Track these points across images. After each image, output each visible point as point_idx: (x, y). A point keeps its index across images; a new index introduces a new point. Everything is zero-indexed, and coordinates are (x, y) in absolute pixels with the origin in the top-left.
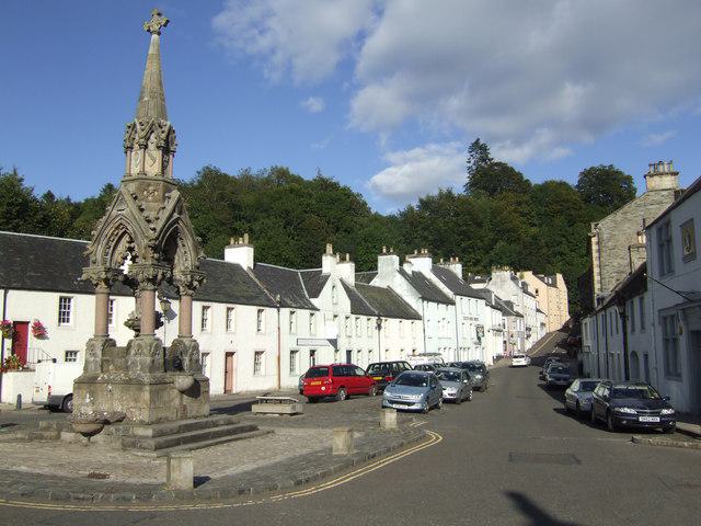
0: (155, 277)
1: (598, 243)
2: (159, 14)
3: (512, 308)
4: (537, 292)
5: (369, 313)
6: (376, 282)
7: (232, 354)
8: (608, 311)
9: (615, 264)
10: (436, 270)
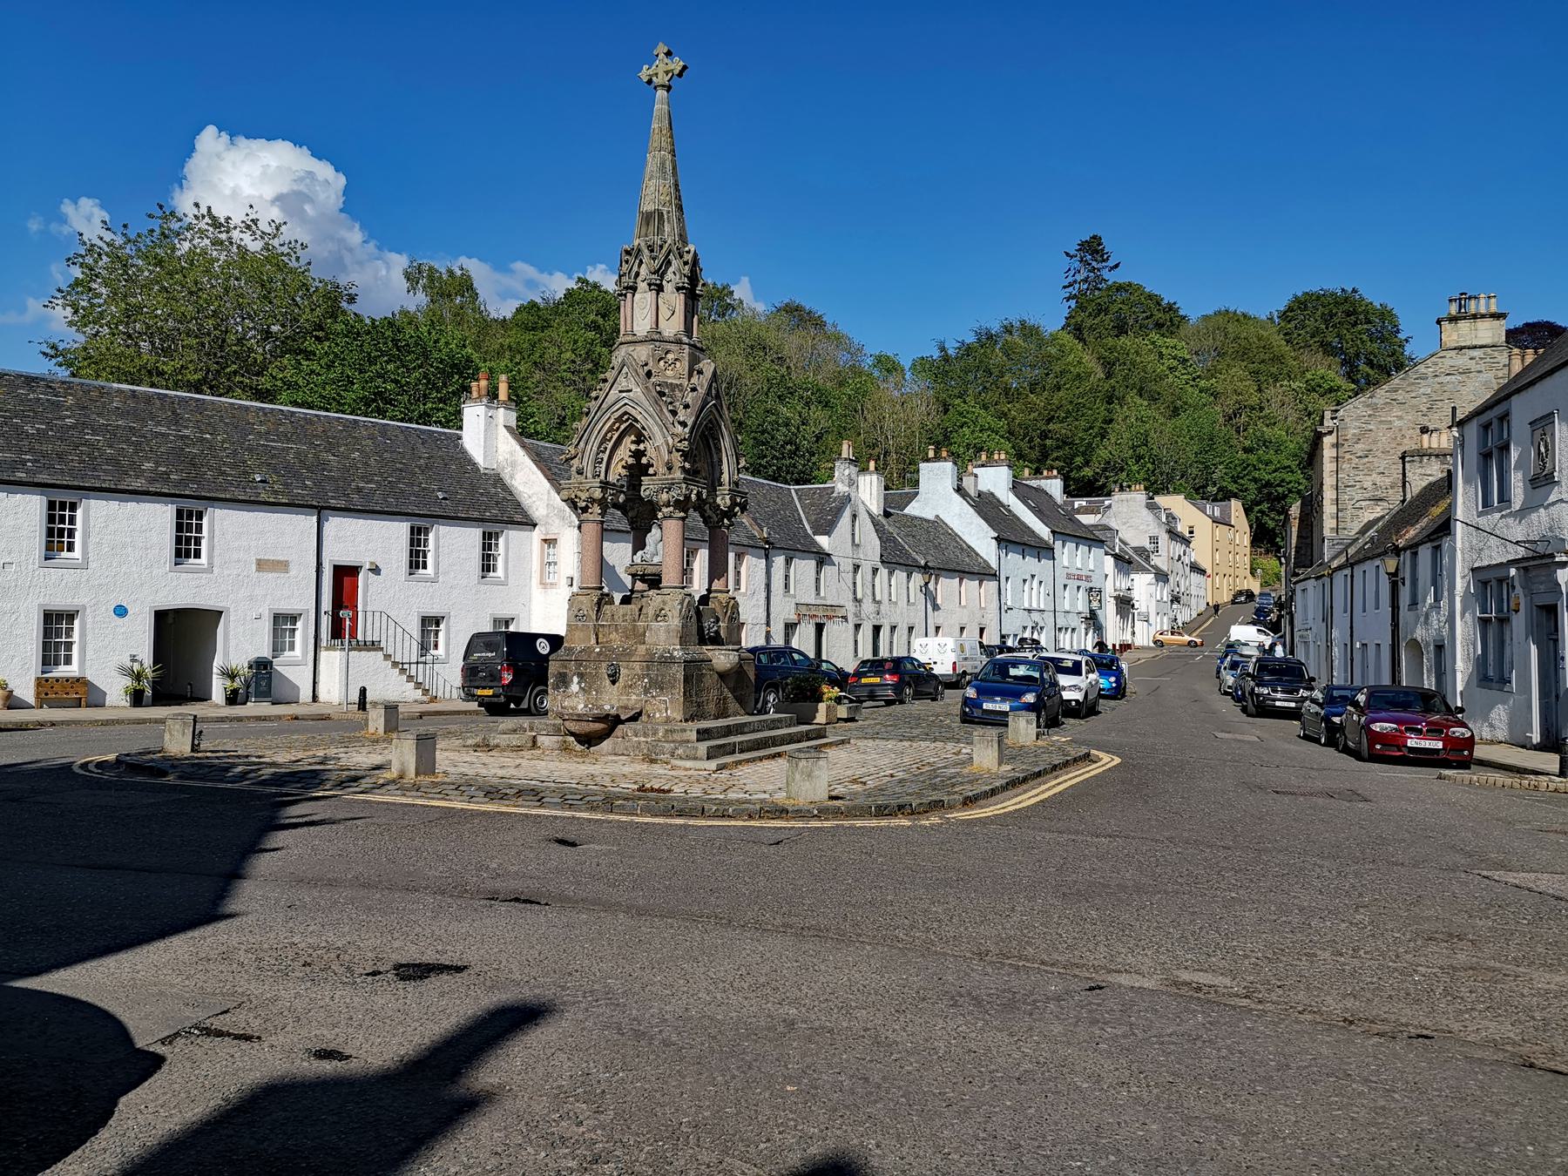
0: (688, 497)
1: (1337, 445)
2: (668, 54)
3: (1147, 559)
4: (1191, 532)
5: (910, 567)
6: (913, 509)
7: (437, 621)
8: (1358, 570)
9: (1368, 484)
10: (1017, 487)
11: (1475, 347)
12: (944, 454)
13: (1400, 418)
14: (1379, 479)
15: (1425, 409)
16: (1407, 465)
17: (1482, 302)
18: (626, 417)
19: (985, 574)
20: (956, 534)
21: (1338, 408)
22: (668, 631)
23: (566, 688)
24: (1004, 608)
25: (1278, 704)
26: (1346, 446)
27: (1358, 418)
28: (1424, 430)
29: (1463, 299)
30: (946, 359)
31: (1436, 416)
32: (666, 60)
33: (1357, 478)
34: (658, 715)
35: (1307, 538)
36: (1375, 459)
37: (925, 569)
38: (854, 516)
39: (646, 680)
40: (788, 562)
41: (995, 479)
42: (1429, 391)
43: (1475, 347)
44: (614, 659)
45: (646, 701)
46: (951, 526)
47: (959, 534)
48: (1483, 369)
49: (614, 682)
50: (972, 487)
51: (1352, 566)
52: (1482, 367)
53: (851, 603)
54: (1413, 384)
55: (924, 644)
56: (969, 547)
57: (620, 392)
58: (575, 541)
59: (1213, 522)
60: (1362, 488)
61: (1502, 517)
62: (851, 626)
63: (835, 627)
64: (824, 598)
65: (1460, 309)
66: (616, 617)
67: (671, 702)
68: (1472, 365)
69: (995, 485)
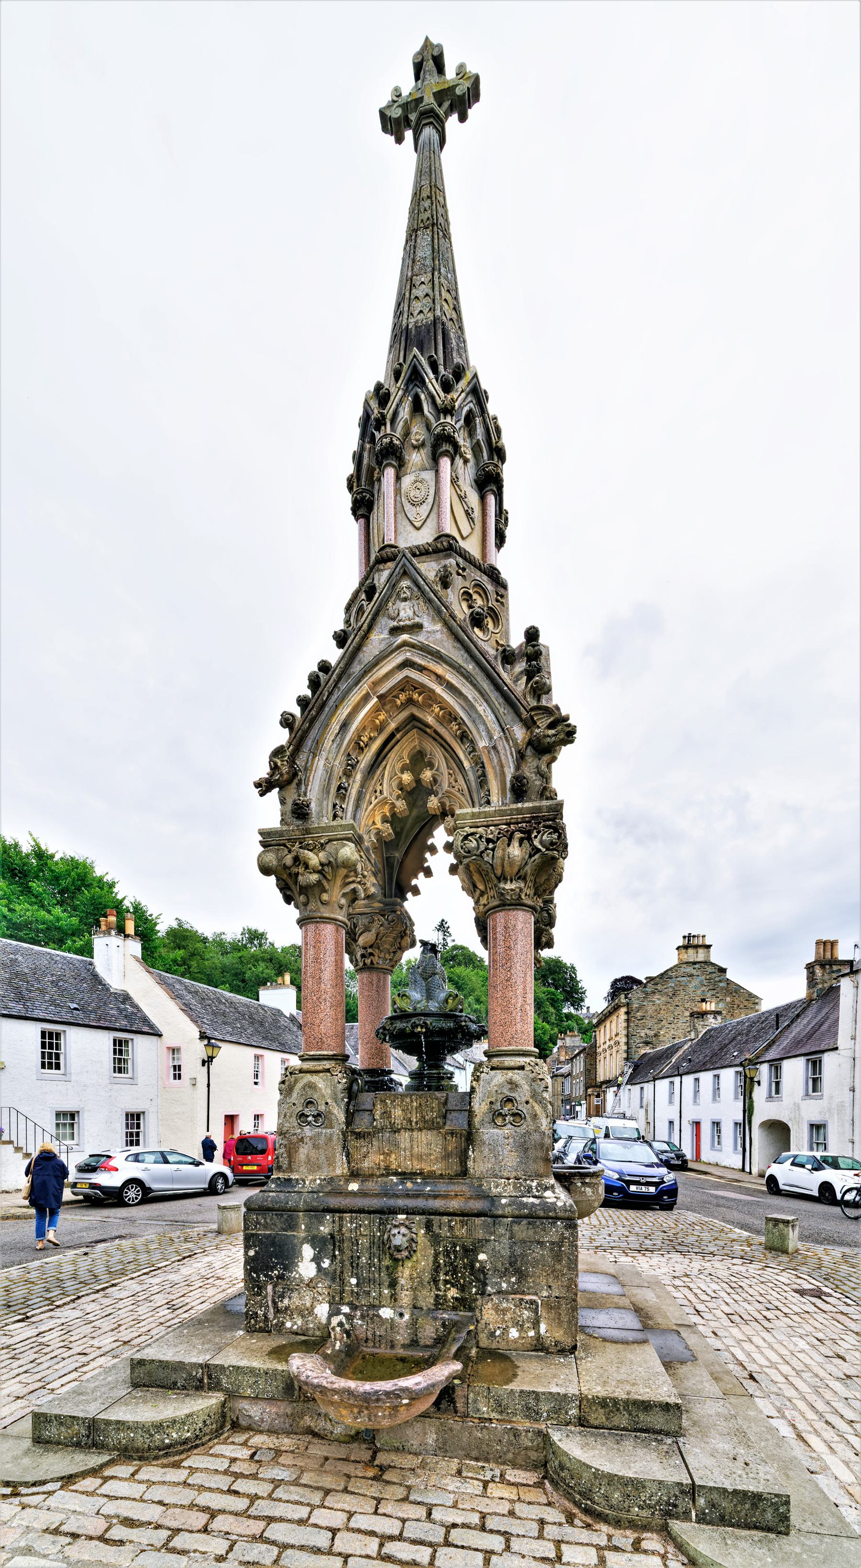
9: (643, 1035)
13: (659, 999)
14: (648, 1032)
23: (286, 1268)
27: (638, 999)
34: (514, 1333)
52: (699, 973)
68: (694, 972)
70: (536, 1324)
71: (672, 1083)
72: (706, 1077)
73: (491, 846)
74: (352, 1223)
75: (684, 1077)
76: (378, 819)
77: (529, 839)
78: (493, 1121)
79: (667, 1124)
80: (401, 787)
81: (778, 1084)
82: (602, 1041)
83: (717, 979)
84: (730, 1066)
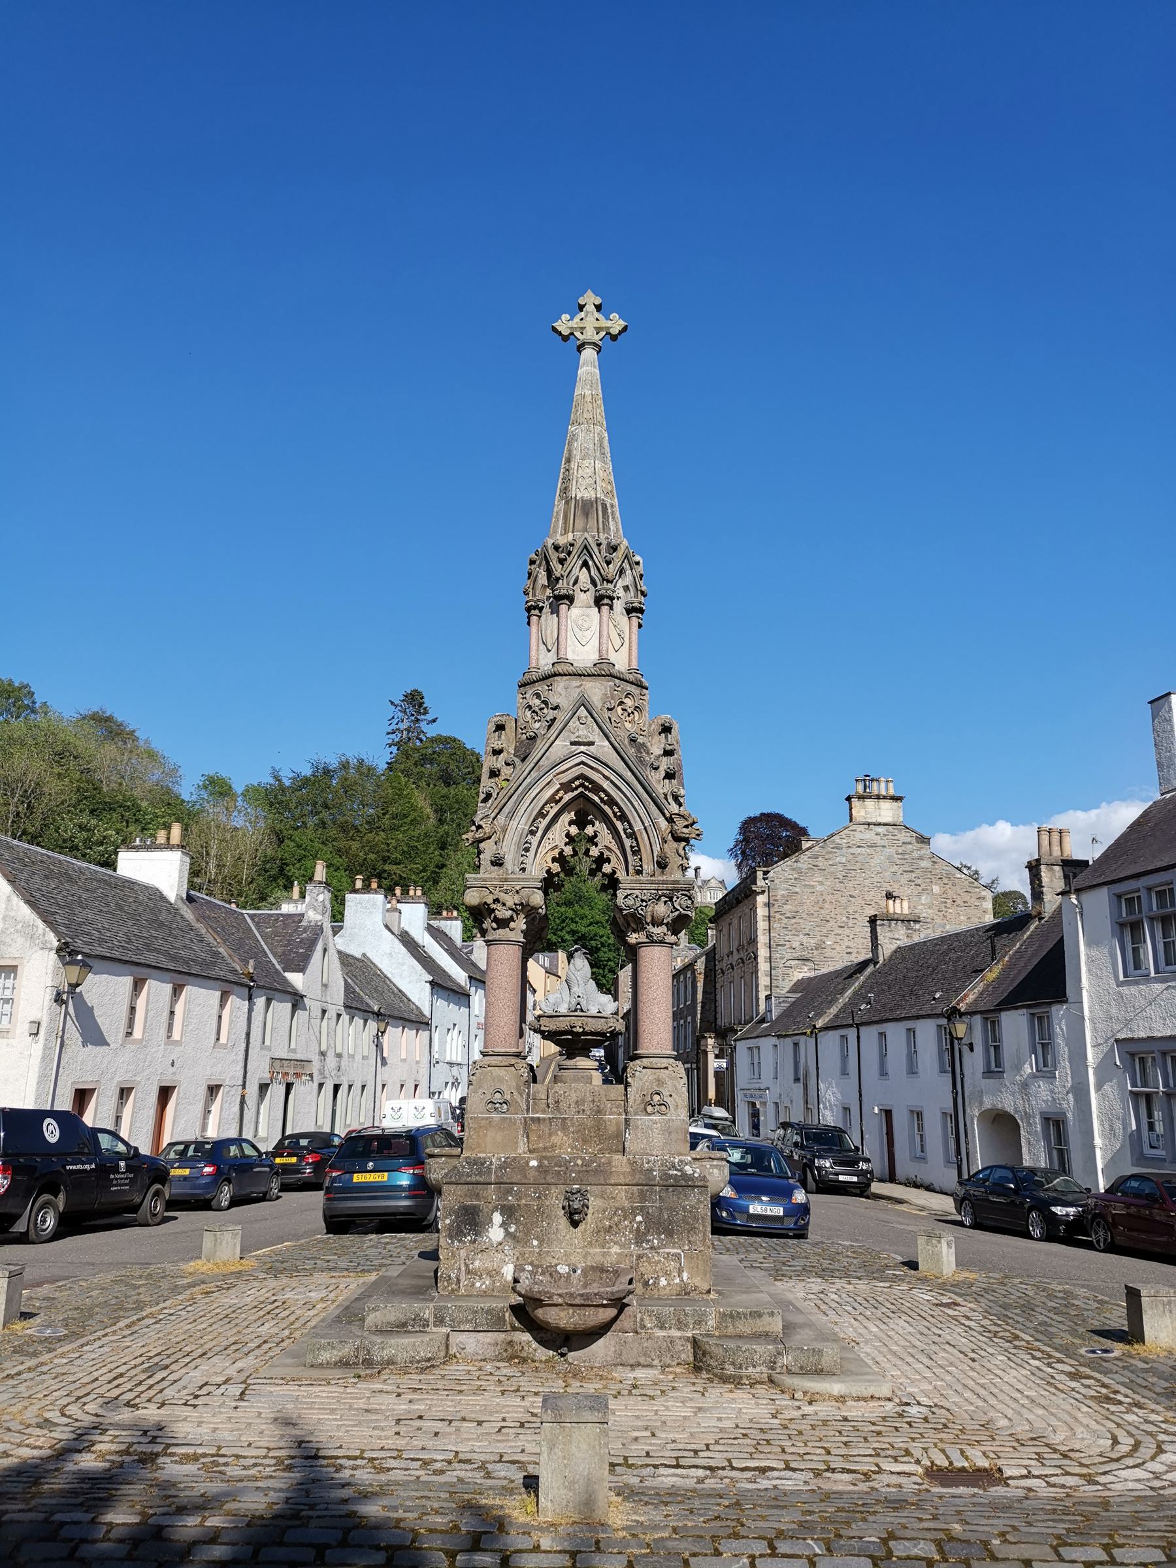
1: (768, 905)
9: (796, 944)
11: (880, 824)
12: (374, 885)
13: (821, 883)
14: (805, 940)
15: (841, 877)
16: (879, 929)
17: (883, 785)
18: (577, 783)
19: (421, 1023)
20: (386, 976)
21: (769, 869)
22: (668, 1131)
24: (434, 1061)
25: (841, 1178)
26: (776, 906)
28: (889, 896)
29: (867, 780)
30: (282, 789)
31: (851, 884)
32: (597, 315)
33: (787, 938)
34: (663, 1282)
35: (710, 994)
36: (801, 921)
37: (378, 1015)
38: (325, 950)
39: (639, 1218)
40: (269, 1001)
41: (414, 916)
42: (844, 860)
43: (880, 824)
44: (574, 1182)
45: (639, 1257)
46: (380, 966)
47: (389, 975)
48: (886, 844)
49: (575, 1224)
50: (396, 923)
51: (858, 1026)
53: (317, 1057)
54: (831, 853)
55: (396, 1107)
56: (400, 991)
57: (572, 744)
58: (50, 971)
59: (546, 972)
60: (791, 948)
61: (1167, 989)
62: (315, 1086)
63: (303, 1088)
64: (294, 1051)
65: (865, 789)
66: (563, 1105)
67: (689, 1257)
68: (877, 839)
69: (410, 924)
70: (680, 1271)
71: (844, 1038)
72: (896, 1033)
73: (644, 904)
74: (535, 1193)
75: (863, 1029)
76: (549, 860)
77: (671, 899)
78: (645, 1110)
79: (202, 1091)
80: (568, 835)
81: (997, 1048)
82: (726, 951)
83: (915, 854)
84: (929, 1016)
